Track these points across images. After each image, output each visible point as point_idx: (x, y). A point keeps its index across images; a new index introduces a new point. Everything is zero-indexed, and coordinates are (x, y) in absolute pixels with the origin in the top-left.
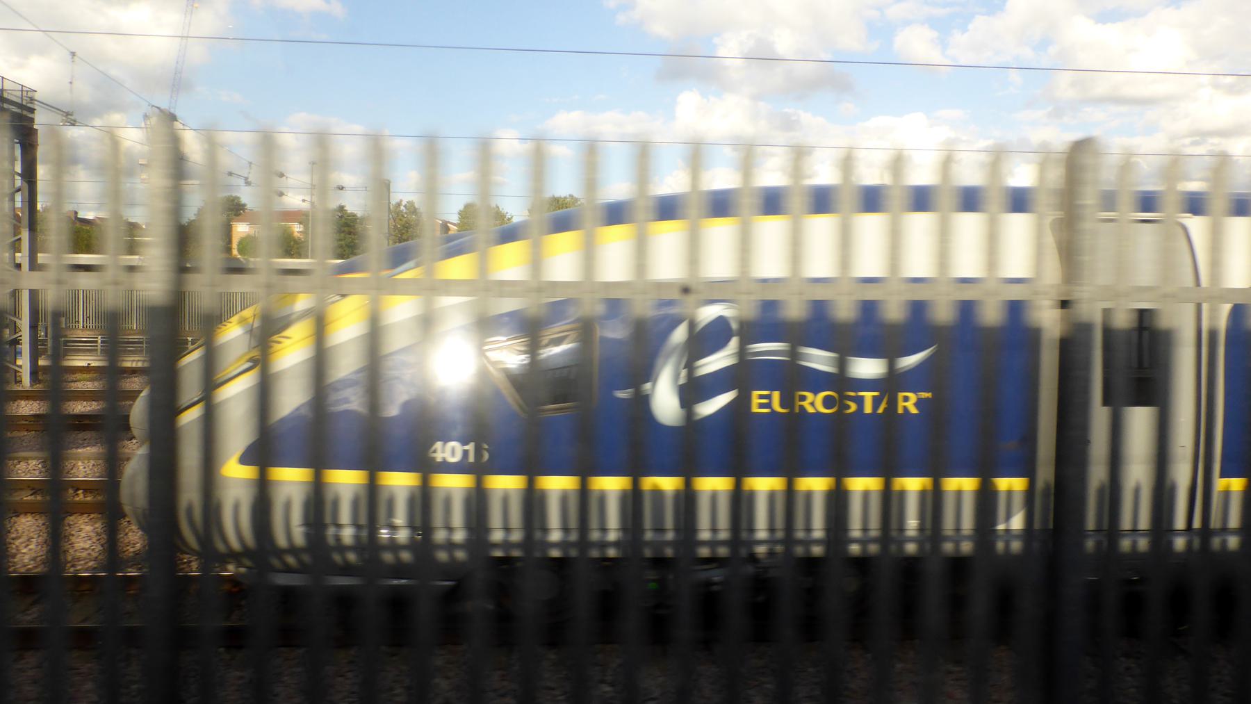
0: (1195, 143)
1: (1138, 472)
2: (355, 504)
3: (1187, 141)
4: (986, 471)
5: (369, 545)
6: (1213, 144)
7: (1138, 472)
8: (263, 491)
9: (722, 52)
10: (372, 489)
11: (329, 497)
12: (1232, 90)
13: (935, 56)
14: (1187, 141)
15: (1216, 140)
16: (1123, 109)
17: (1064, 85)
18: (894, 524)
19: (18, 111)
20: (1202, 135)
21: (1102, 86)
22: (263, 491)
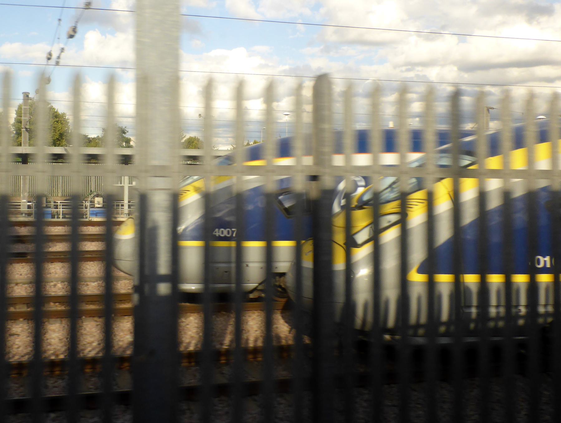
0: (408, 70)
1: (363, 273)
2: (498, 292)
3: (404, 68)
4: (508, 273)
5: (510, 316)
6: (418, 71)
7: (363, 273)
8: (431, 285)
9: (115, 6)
10: (508, 284)
11: (514, 287)
12: (428, 39)
13: (251, 13)
14: (404, 68)
15: (420, 68)
16: (366, 48)
17: (330, 34)
18: (436, 307)
19: (477, 89)
20: (411, 65)
21: (353, 34)
22: (431, 285)
